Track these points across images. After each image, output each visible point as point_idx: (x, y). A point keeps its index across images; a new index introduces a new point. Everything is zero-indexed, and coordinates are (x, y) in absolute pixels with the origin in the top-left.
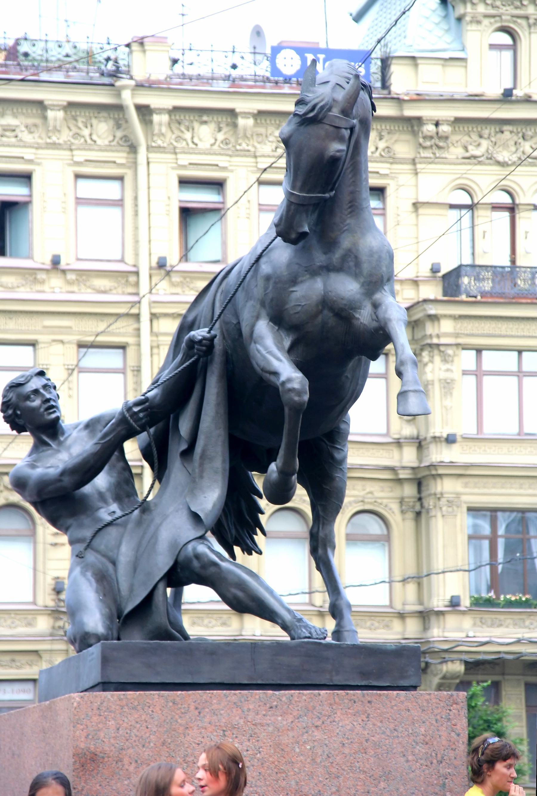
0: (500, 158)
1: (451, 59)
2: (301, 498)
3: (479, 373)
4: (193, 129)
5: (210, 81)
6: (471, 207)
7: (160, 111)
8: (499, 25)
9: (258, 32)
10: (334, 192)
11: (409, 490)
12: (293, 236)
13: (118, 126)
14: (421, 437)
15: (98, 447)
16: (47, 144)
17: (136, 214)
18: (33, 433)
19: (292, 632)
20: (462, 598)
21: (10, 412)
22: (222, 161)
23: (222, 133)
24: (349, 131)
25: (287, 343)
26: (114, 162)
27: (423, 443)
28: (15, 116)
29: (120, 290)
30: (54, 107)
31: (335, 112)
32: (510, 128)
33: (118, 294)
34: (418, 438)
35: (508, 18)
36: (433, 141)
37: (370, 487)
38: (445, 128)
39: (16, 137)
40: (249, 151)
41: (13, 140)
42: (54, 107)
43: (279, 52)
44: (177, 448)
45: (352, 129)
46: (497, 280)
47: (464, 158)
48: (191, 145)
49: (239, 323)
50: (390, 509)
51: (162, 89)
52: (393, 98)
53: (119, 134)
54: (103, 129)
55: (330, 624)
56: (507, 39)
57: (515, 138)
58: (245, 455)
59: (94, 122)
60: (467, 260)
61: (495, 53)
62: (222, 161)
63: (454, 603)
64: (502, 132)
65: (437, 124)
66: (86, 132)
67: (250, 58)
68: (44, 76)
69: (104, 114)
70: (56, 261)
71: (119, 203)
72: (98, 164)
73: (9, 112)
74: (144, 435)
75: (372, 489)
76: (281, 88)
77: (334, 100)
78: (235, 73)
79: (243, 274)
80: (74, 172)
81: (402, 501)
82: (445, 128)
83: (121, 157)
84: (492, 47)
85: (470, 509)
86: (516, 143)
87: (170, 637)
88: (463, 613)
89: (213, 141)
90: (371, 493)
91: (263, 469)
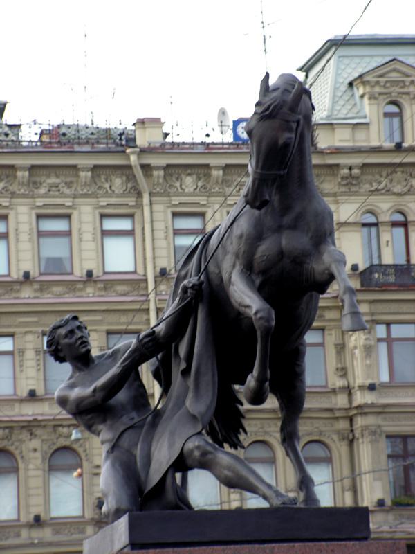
0: (395, 190)
1: (358, 124)
2: (272, 402)
3: (389, 340)
4: (181, 180)
5: (192, 146)
6: (376, 225)
7: (158, 168)
8: (389, 99)
9: (223, 113)
10: (286, 171)
11: (343, 425)
12: (257, 204)
13: (128, 180)
14: (350, 387)
15: (121, 369)
16: (82, 194)
17: (144, 240)
18: (71, 364)
19: (271, 501)
20: (386, 500)
21: (53, 348)
22: (203, 200)
23: (201, 181)
24: (296, 124)
25: (258, 282)
26: (127, 205)
27: (352, 391)
28: (57, 176)
29: (135, 293)
30: (83, 169)
31: (285, 110)
32: (401, 169)
33: (133, 296)
34: (348, 387)
35: (396, 94)
36: (348, 180)
37: (317, 424)
38: (356, 171)
39: (59, 191)
40: (220, 192)
41: (57, 193)
42: (83, 169)
43: (239, 124)
44: (177, 368)
45: (298, 122)
46: (398, 274)
47: (370, 191)
48: (180, 190)
49: (220, 273)
50: (332, 439)
51: (159, 153)
52: (319, 152)
53: (130, 185)
54: (118, 182)
55: (302, 496)
56: (394, 109)
57: (405, 175)
58: (230, 368)
59: (113, 177)
60: (376, 262)
61: (387, 120)
62: (203, 200)
63: (381, 503)
64: (396, 172)
65: (350, 168)
66: (107, 185)
67: (218, 129)
68: (77, 148)
69: (119, 172)
70: (90, 274)
71: (130, 233)
72: (117, 207)
73: (53, 174)
74: (154, 359)
75: (317, 425)
76: (241, 148)
77: (284, 102)
78: (208, 140)
79: (221, 236)
80: (99, 213)
81: (338, 432)
82: (356, 171)
83: (131, 201)
84: (386, 115)
85: (388, 437)
86: (406, 180)
87: (177, 507)
88: (388, 511)
89: (195, 187)
90: (317, 428)
91: (242, 382)
